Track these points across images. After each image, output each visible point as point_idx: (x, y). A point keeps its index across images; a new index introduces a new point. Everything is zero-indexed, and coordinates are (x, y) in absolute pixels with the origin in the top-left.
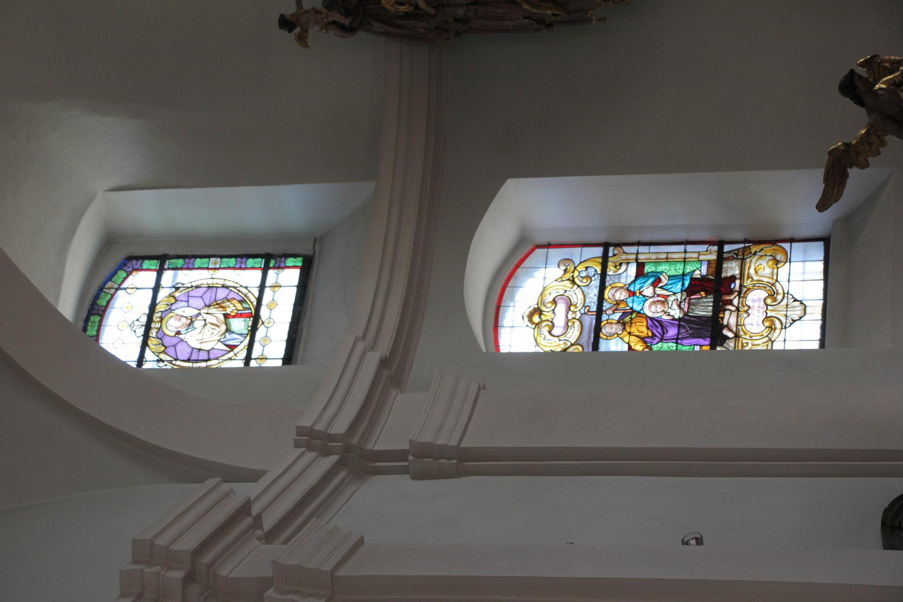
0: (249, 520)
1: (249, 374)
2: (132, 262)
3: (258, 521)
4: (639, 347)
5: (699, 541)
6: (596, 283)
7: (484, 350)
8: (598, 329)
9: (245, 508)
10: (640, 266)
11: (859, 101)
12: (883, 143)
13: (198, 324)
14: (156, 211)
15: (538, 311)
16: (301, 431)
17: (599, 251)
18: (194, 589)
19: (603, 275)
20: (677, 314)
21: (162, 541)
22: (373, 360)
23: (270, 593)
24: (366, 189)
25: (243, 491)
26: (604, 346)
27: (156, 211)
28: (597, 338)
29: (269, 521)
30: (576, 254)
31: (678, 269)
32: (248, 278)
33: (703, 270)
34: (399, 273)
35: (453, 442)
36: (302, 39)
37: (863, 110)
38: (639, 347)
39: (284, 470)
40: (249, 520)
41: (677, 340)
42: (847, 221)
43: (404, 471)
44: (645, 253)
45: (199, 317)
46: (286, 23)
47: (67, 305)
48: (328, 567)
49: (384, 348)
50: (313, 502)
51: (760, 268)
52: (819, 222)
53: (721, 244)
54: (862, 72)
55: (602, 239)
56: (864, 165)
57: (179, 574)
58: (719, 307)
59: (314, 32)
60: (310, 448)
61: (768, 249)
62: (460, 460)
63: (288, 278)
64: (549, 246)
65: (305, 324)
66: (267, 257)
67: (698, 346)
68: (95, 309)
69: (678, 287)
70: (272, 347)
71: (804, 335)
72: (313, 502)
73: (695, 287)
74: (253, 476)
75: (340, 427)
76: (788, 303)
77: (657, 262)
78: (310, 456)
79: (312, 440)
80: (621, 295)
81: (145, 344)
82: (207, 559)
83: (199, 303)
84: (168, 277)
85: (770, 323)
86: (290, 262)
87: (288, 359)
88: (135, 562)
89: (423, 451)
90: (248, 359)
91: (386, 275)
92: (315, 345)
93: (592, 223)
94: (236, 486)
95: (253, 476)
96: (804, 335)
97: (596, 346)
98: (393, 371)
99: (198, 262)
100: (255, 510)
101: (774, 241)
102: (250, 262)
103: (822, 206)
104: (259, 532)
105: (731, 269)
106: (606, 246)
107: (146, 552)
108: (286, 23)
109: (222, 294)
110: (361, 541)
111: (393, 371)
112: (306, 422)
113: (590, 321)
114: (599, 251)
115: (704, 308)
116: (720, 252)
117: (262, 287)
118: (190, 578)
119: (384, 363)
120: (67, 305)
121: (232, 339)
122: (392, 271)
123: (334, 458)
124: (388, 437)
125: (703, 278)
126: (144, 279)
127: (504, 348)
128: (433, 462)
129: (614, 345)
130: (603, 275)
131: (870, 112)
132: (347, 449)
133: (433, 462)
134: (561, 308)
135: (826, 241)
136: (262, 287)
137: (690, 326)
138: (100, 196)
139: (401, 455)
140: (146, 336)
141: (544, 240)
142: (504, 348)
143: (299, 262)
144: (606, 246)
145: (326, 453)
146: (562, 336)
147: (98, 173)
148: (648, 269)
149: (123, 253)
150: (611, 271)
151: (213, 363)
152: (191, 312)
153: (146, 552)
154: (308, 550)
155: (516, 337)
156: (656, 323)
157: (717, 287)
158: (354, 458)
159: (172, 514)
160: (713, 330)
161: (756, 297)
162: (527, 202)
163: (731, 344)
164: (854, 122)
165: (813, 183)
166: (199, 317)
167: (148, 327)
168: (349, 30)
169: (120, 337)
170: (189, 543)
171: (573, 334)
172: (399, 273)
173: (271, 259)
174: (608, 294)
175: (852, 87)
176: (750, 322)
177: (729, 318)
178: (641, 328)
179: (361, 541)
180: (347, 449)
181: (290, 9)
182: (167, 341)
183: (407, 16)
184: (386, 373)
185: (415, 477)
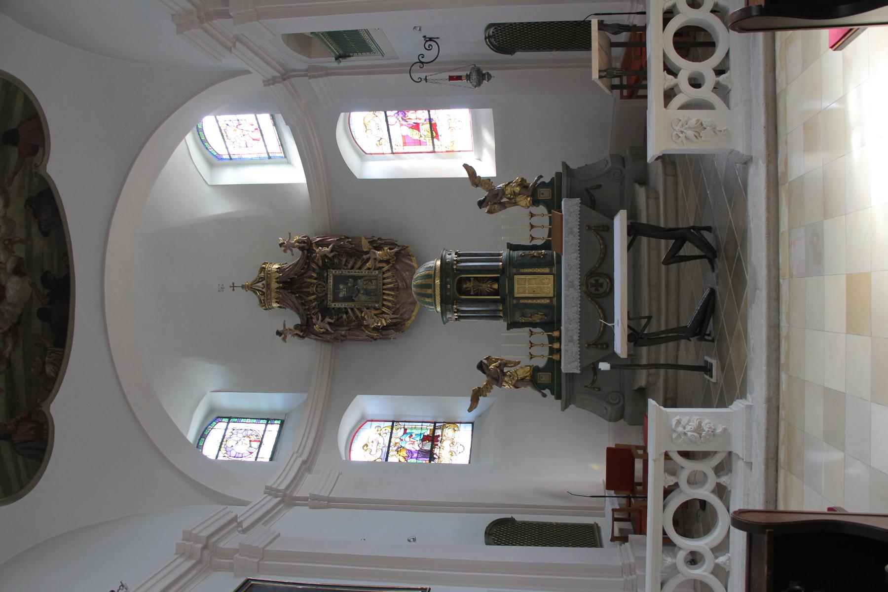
0: (235, 524)
1: (256, 464)
2: (219, 419)
3: (240, 524)
4: (403, 460)
5: (414, 540)
6: (389, 435)
7: (344, 458)
8: (388, 453)
9: (235, 519)
10: (405, 430)
11: (484, 372)
12: (492, 388)
13: (240, 443)
14: (228, 400)
15: (367, 445)
16: (267, 488)
17: (390, 424)
18: (206, 552)
19: (391, 433)
20: (418, 449)
21: (194, 532)
22: (299, 461)
23: (237, 555)
24: (305, 395)
25: (238, 511)
26: (390, 460)
27: (228, 400)
28: (387, 456)
29: (245, 525)
30: (382, 424)
31: (419, 432)
32: (259, 427)
33: (428, 433)
34: (315, 428)
35: (326, 495)
36: (284, 339)
37: (485, 376)
38: (403, 460)
39: (260, 501)
40: (235, 524)
41: (417, 458)
42: (480, 416)
43: (306, 505)
44: (407, 425)
45: (242, 442)
46: (279, 333)
47: (191, 436)
48: (262, 546)
49: (305, 457)
50: (266, 518)
51: (448, 432)
52: (470, 416)
53: (435, 423)
54: (485, 362)
55: (392, 419)
56: (485, 396)
57: (200, 546)
58: (433, 447)
59: (289, 337)
60: (270, 495)
61: (452, 425)
62: (329, 502)
63: (274, 428)
64: (372, 421)
65: (278, 445)
66: (268, 420)
67: (424, 461)
68: (202, 436)
69: (418, 438)
70: (265, 454)
71: (463, 458)
72: (266, 518)
73: (425, 438)
74: (244, 503)
75: (283, 487)
76: (457, 446)
77: (412, 429)
78: (270, 497)
79: (271, 491)
80: (398, 440)
81: (220, 450)
82: (214, 540)
83: (240, 435)
84: (231, 425)
85: (452, 453)
86: (276, 422)
87: (271, 459)
88: (183, 540)
89: (314, 498)
90: (256, 458)
91: (308, 429)
92: (282, 454)
93: (389, 413)
94: (230, 508)
95: (244, 503)
96: (463, 458)
97: (387, 460)
98: (307, 466)
99: (243, 420)
100: (239, 520)
101: (454, 423)
102: (262, 421)
103: (470, 410)
104: (240, 529)
105: (438, 432)
106: (393, 422)
107: (188, 536)
108: (279, 333)
109: (250, 432)
110: (279, 535)
111: (307, 466)
112: (269, 484)
113: (385, 450)
114: (390, 424)
115: (427, 446)
116: (435, 426)
117: (265, 431)
118: (205, 547)
119: (304, 462)
120: (191, 436)
121: (251, 450)
122: (311, 427)
123: (279, 499)
124: (302, 491)
125: (428, 436)
126: (221, 426)
127: (353, 459)
128: (318, 502)
129: (393, 458)
130: (391, 433)
131: (488, 376)
132: (285, 495)
133: (318, 502)
134: (375, 443)
135: (472, 423)
136: (265, 431)
137: (422, 453)
138: (208, 394)
139: (306, 499)
140: (220, 447)
141: (370, 418)
142: (353, 459)
143: (279, 422)
144: (393, 422)
145: (276, 497)
146: (375, 455)
147: (209, 386)
148: (408, 431)
149: (216, 415)
150: (394, 431)
151: (243, 459)
152: (238, 439)
153: (188, 536)
154: (256, 539)
155: (358, 455)
156: (410, 452)
157: (433, 439)
158: (287, 499)
159: (202, 518)
160: (431, 455)
161: (446, 444)
162: (367, 404)
163: (436, 461)
164: (481, 380)
165: (467, 402)
166: (242, 442)
167: (221, 444)
168: (302, 337)
169: (210, 449)
170: (205, 534)
171: (379, 454)
172: (315, 428)
173: (269, 421)
174: (393, 440)
175: (481, 367)
176: (445, 454)
177: (436, 451)
178: (404, 453)
179: (279, 535)
180: (285, 495)
181: (281, 329)
182: (228, 449)
183: (324, 333)
184: (304, 466)
185: (311, 508)
